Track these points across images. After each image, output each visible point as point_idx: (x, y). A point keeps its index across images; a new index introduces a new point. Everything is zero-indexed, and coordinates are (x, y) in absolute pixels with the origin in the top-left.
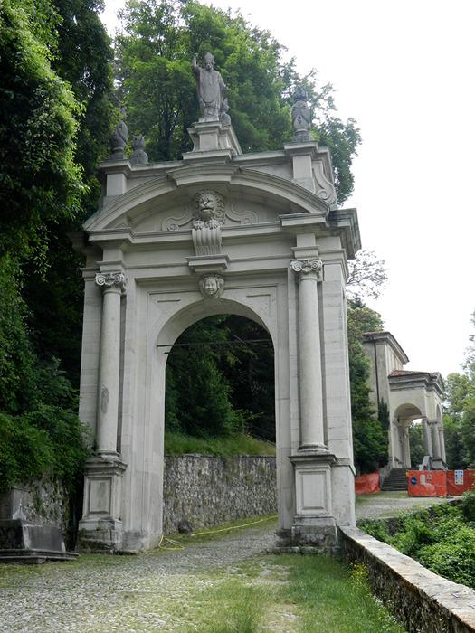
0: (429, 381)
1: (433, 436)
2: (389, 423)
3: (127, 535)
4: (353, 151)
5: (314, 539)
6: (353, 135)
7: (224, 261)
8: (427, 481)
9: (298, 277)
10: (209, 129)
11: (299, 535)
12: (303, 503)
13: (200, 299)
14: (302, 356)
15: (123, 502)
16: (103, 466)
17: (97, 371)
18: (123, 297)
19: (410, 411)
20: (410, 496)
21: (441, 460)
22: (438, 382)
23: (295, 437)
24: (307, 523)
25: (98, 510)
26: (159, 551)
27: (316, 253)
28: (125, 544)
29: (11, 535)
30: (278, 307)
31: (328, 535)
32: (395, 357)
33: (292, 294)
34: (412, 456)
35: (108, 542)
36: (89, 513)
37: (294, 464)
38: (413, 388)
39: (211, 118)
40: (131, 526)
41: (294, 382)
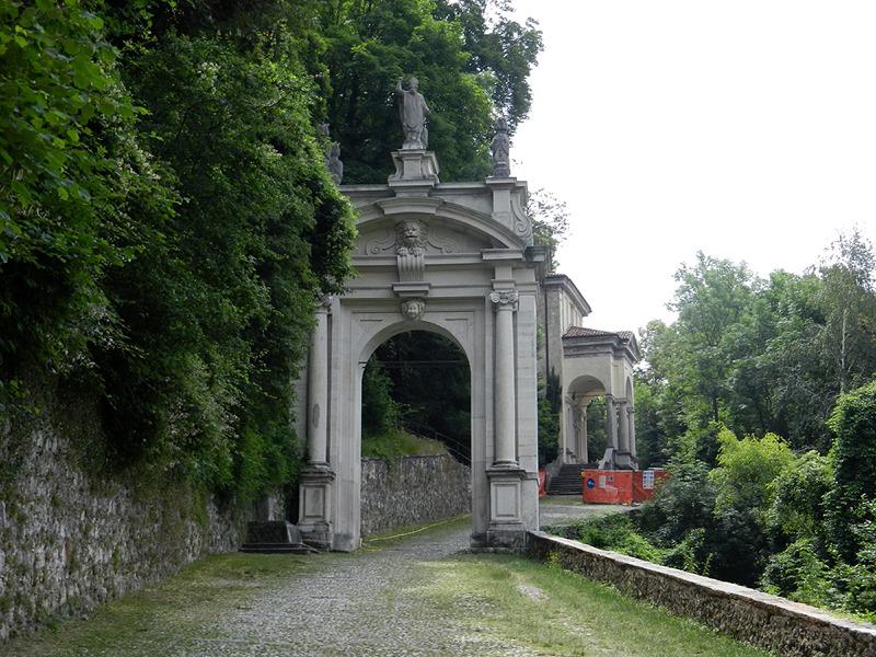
0: (617, 344)
1: (619, 421)
2: (560, 403)
3: (337, 536)
4: (532, 59)
5: (506, 542)
6: (532, 42)
7: (426, 288)
8: (608, 483)
9: (495, 308)
10: (413, 155)
11: (493, 538)
12: (496, 511)
13: (401, 320)
14: (498, 381)
15: (332, 507)
16: (317, 475)
17: (305, 387)
18: (329, 316)
19: (589, 385)
20: (585, 503)
21: (629, 454)
22: (630, 345)
23: (489, 453)
24: (500, 528)
25: (313, 514)
26: (361, 553)
27: (512, 285)
28: (336, 544)
29: (278, 532)
30: (475, 332)
31: (518, 539)
32: (572, 307)
33: (489, 322)
34: (590, 445)
35: (324, 542)
36: (304, 516)
37: (489, 477)
38: (595, 354)
39: (416, 144)
40: (340, 528)
41: (489, 403)
